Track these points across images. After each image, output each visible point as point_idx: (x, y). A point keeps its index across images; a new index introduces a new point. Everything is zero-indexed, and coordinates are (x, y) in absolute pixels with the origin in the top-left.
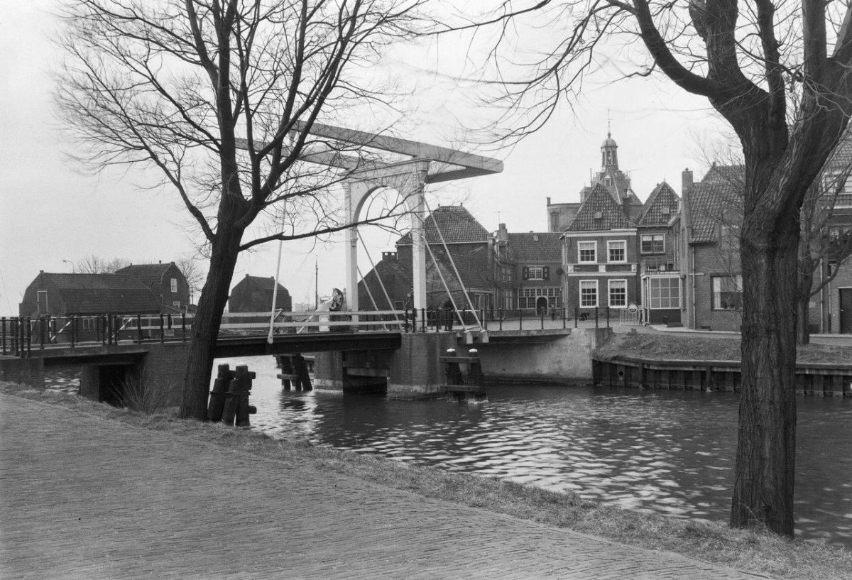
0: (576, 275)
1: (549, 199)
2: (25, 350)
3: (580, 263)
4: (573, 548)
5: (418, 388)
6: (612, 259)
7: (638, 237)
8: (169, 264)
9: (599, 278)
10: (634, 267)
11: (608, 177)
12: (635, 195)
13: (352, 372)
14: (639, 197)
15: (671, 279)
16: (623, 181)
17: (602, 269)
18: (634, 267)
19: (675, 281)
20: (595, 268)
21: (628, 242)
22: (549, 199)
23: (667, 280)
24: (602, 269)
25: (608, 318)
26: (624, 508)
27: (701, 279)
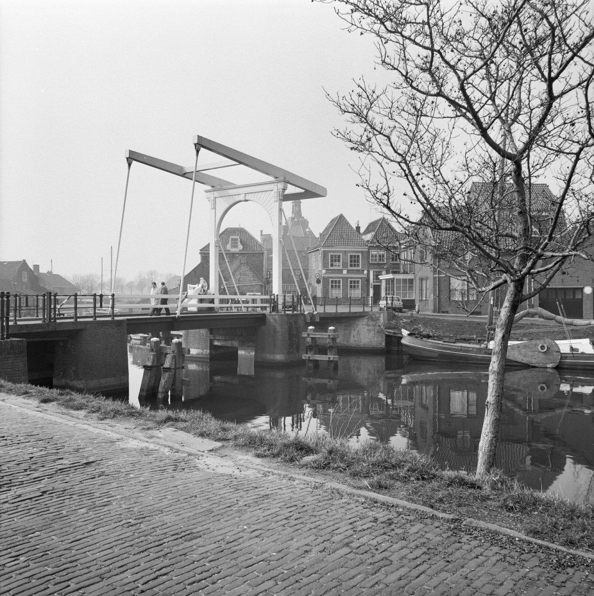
0: (327, 275)
1: (262, 231)
2: (11, 323)
3: (349, 268)
4: (76, 437)
5: (279, 357)
6: (351, 266)
7: (368, 252)
8: (21, 262)
9: (343, 278)
10: (365, 272)
11: (296, 220)
12: (311, 232)
13: (216, 343)
14: (314, 233)
15: (403, 279)
16: (305, 223)
17: (345, 272)
18: (365, 272)
19: (411, 281)
20: (340, 271)
21: (362, 255)
22: (262, 231)
23: (400, 279)
24: (345, 272)
25: (337, 305)
26: (30, 401)
27: (443, 279)
